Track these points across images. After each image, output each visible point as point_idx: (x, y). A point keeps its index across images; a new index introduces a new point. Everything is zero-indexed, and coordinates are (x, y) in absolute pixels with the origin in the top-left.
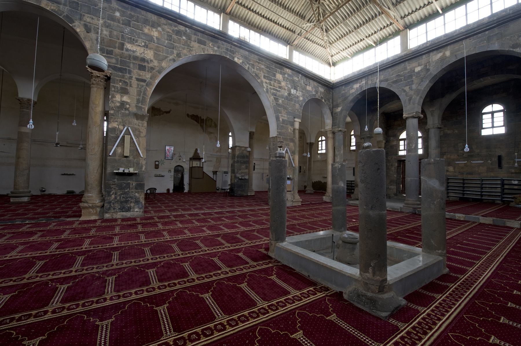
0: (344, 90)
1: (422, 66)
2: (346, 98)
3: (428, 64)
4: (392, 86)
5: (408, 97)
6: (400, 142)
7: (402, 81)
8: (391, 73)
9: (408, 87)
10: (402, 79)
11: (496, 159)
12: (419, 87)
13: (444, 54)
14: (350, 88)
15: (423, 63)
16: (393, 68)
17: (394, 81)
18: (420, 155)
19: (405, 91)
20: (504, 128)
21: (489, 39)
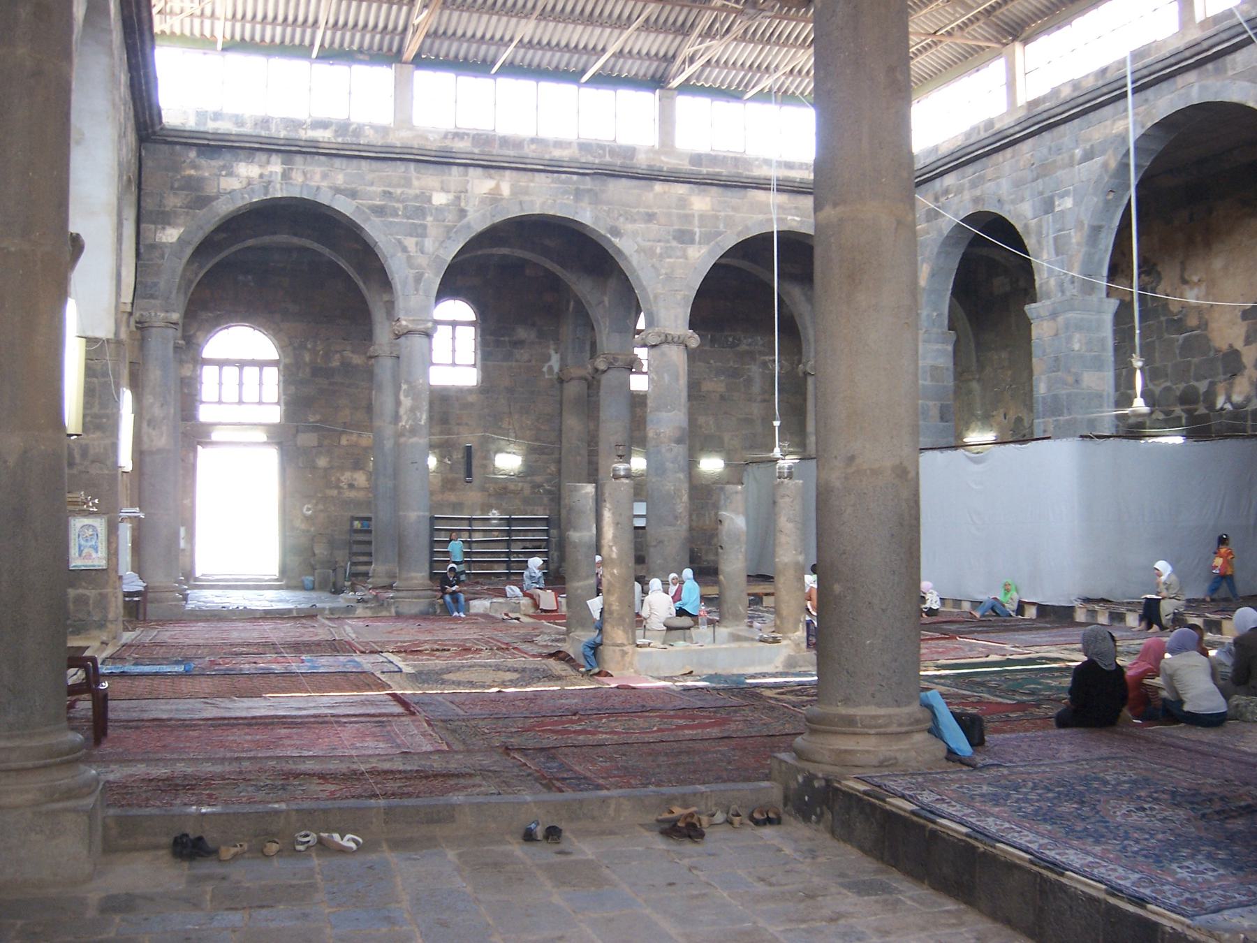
0: (195, 167)
1: (451, 196)
2: (203, 201)
3: (463, 195)
7: (397, 215)
8: (369, 177)
9: (414, 240)
10: (398, 208)
11: (458, 455)
12: (441, 252)
13: (498, 186)
14: (224, 167)
15: (452, 188)
16: (375, 164)
17: (377, 206)
18: (488, 458)
19: (405, 249)
21: (578, 194)
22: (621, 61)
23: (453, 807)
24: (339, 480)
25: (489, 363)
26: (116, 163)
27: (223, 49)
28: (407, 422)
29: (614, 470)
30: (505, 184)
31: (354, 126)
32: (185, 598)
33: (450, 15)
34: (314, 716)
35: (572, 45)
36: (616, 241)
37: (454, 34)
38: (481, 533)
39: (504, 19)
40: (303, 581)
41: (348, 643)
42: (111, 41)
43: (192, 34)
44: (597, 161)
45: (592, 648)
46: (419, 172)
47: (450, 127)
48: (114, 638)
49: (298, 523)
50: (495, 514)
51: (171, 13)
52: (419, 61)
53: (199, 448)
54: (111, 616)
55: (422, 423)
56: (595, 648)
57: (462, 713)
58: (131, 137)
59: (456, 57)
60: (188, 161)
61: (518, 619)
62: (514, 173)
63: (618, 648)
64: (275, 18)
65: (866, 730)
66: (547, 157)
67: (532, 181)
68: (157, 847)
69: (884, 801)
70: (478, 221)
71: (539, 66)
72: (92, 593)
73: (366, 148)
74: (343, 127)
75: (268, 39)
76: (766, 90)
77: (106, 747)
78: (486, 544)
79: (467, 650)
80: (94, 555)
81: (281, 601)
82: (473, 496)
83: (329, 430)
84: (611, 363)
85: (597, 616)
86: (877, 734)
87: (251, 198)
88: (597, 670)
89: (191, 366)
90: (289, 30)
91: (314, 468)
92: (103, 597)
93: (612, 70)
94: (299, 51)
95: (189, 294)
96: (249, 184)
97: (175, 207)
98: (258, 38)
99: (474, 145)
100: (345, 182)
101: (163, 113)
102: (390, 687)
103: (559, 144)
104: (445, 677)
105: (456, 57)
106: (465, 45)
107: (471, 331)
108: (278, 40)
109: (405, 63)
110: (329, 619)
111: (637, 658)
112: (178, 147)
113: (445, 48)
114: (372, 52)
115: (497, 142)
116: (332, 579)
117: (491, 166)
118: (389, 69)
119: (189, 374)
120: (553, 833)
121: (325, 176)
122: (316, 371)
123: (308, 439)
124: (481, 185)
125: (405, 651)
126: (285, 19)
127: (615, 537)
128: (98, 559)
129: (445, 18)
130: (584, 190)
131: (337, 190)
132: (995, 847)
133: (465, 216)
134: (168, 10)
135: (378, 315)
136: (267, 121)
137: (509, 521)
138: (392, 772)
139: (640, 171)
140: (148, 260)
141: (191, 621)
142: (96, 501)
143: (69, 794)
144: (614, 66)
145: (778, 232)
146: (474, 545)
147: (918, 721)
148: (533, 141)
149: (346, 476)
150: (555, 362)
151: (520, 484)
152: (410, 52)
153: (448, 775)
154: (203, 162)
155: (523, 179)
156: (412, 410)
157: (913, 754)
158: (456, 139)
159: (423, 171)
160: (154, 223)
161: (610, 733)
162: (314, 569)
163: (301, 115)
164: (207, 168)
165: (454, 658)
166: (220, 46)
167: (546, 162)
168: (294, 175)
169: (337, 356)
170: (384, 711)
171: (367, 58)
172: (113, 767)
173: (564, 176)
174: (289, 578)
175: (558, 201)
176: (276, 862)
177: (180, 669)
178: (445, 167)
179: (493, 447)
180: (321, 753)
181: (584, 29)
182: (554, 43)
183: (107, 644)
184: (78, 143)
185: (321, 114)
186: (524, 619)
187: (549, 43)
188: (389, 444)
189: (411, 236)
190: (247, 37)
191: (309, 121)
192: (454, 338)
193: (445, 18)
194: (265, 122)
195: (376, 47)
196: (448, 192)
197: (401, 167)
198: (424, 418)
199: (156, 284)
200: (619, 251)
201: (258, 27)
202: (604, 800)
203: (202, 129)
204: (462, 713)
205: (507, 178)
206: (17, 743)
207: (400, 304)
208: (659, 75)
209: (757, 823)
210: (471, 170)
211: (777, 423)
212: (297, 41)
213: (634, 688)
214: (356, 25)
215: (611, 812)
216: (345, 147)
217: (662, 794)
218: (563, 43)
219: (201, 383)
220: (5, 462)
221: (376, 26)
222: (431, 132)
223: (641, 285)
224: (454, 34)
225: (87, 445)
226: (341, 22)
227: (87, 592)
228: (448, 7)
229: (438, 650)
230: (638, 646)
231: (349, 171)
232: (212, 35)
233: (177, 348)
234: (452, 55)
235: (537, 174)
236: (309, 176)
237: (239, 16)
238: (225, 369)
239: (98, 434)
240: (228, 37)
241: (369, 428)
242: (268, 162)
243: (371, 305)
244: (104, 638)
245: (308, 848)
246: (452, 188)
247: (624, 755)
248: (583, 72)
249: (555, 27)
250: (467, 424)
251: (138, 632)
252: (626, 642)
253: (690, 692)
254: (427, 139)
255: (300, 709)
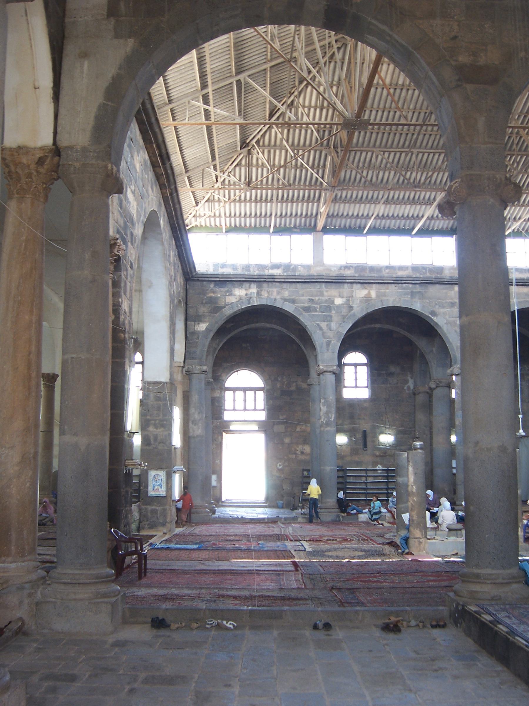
0: (214, 292)
1: (344, 300)
2: (217, 309)
4: (302, 314)
5: (327, 340)
6: (226, 392)
7: (317, 311)
8: (301, 292)
9: (326, 323)
10: (317, 308)
11: (359, 436)
12: (340, 330)
13: (369, 293)
14: (228, 291)
15: (345, 295)
17: (306, 307)
18: (375, 437)
19: (321, 329)
20: (367, 390)
21: (413, 294)
22: (433, 222)
23: (282, 611)
24: (296, 450)
25: (375, 385)
26: (168, 296)
27: (226, 232)
28: (324, 420)
29: (414, 445)
30: (373, 292)
31: (293, 266)
32: (214, 512)
33: (339, 206)
34: (248, 570)
35: (406, 215)
36: (434, 318)
37: (342, 215)
38: (354, 478)
39: (368, 205)
40: (277, 504)
41: (287, 536)
42: (162, 238)
43: (210, 225)
44: (422, 276)
45: (404, 540)
46: (327, 288)
47: (343, 262)
48: (170, 531)
49: (275, 473)
50: (379, 467)
51: (200, 216)
52: (326, 230)
53: (224, 434)
54: (168, 520)
55: (332, 420)
56: (406, 540)
57: (322, 570)
58: (180, 280)
59: (345, 226)
60: (210, 289)
61: (382, 524)
62: (378, 285)
63: (416, 540)
64: (251, 214)
65: (485, 581)
66: (394, 276)
67: (388, 289)
68: (146, 623)
69: (481, 616)
70: (359, 312)
71: (389, 227)
72: (159, 508)
73: (299, 277)
74: (287, 267)
75: (248, 225)
76: (516, 230)
77: (144, 581)
78: (375, 484)
79: (345, 540)
80: (160, 489)
81: (263, 514)
82: (367, 457)
83: (291, 423)
84: (438, 384)
85: (407, 522)
86: (491, 583)
87: (242, 306)
88: (407, 551)
89: (219, 391)
90: (258, 220)
91: (282, 443)
92: (165, 510)
93: (428, 227)
94: (263, 229)
95: (215, 356)
96: (240, 299)
97: (204, 313)
98: (243, 225)
99: (356, 272)
100: (289, 295)
101: (196, 266)
102: (294, 557)
103: (401, 268)
104: (326, 553)
105: (345, 226)
106: (349, 220)
107: (365, 369)
108: (253, 225)
109: (318, 232)
110: (283, 523)
111: (427, 544)
112: (205, 283)
113: (338, 222)
114: (301, 227)
115: (368, 270)
116: (292, 502)
117: (365, 282)
118: (310, 236)
119: (218, 395)
120: (327, 626)
121: (278, 293)
122: (285, 393)
123: (280, 428)
124: (360, 293)
125: (313, 540)
126: (256, 214)
127: (414, 480)
128: (162, 492)
129: (337, 207)
130: (416, 292)
131: (285, 300)
132: (515, 638)
133: (352, 310)
134: (198, 215)
135: (311, 363)
136: (249, 267)
137: (387, 471)
138: (273, 597)
139: (445, 280)
140: (191, 340)
141: (213, 523)
142: (146, 464)
143: (105, 595)
144: (430, 224)
145: (518, 310)
146: (368, 484)
147: (514, 577)
148: (387, 267)
149: (300, 448)
150: (411, 384)
151: (393, 451)
152: (320, 225)
153: (297, 599)
154: (217, 289)
155: (383, 289)
156: (327, 413)
157: (510, 594)
158: (346, 269)
159: (329, 287)
160: (194, 321)
161: (391, 582)
162: (283, 497)
163: (265, 261)
164: (219, 292)
165: (336, 544)
166: (224, 231)
167: (394, 279)
168: (263, 293)
169: (294, 384)
170: (284, 569)
171: (298, 230)
172: (142, 589)
173: (404, 285)
174: (270, 502)
175: (402, 299)
176: (195, 632)
177: (195, 546)
178: (341, 284)
179: (378, 431)
180: (241, 587)
181: (411, 207)
182: (395, 215)
183: (166, 534)
184: (150, 287)
185: (276, 260)
186: (386, 524)
187: (393, 216)
188: (318, 431)
189: (324, 321)
190: (238, 225)
191: (270, 265)
192: (356, 373)
193: (337, 207)
194: (248, 267)
195: (303, 224)
196: (342, 297)
197: (318, 286)
198: (333, 417)
199: (195, 352)
200: (436, 324)
201: (243, 220)
202: (356, 612)
203: (216, 273)
204: (322, 570)
205: (374, 288)
206: (84, 572)
207: (319, 357)
208: (454, 227)
209: (433, 627)
210: (355, 285)
211: (520, 416)
212: (263, 225)
213: (419, 561)
214: (291, 214)
215: (360, 617)
216: (288, 277)
217: (386, 610)
218: (400, 215)
219: (225, 400)
220: (80, 449)
221: (302, 214)
222: (333, 266)
223: (449, 341)
224: (342, 215)
225: (157, 434)
226: (284, 214)
227: (157, 508)
228: (338, 202)
229: (330, 540)
230: (428, 539)
231: (291, 289)
232: (221, 225)
233: (208, 383)
234: (342, 226)
235: (390, 285)
236: (270, 293)
237: (233, 215)
238: (237, 392)
239: (162, 429)
240: (228, 225)
241: (307, 421)
242: (250, 288)
243: (308, 358)
244: (165, 531)
245: (211, 627)
246: (345, 295)
247: (390, 593)
248: (413, 228)
249: (395, 207)
250: (364, 419)
251: (184, 528)
252: (421, 537)
253: (449, 564)
254: (331, 270)
255: (244, 567)
